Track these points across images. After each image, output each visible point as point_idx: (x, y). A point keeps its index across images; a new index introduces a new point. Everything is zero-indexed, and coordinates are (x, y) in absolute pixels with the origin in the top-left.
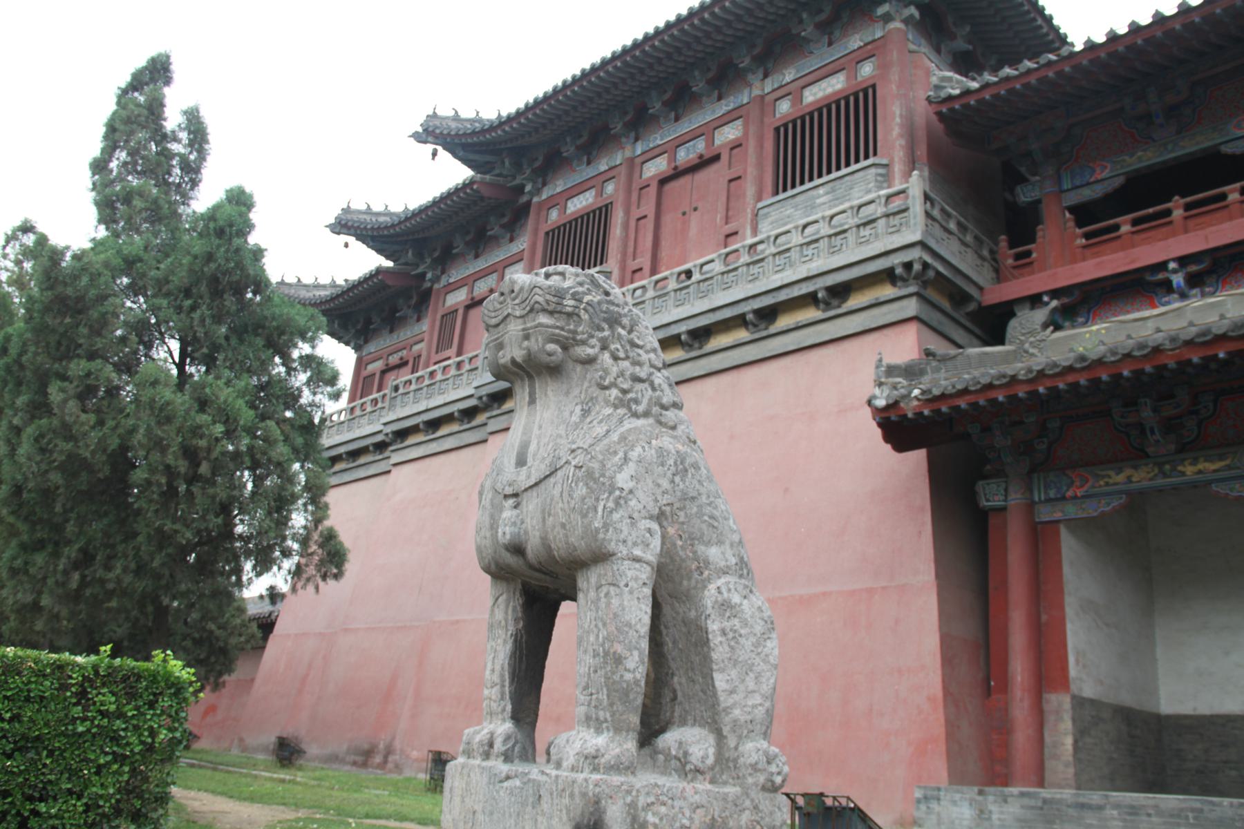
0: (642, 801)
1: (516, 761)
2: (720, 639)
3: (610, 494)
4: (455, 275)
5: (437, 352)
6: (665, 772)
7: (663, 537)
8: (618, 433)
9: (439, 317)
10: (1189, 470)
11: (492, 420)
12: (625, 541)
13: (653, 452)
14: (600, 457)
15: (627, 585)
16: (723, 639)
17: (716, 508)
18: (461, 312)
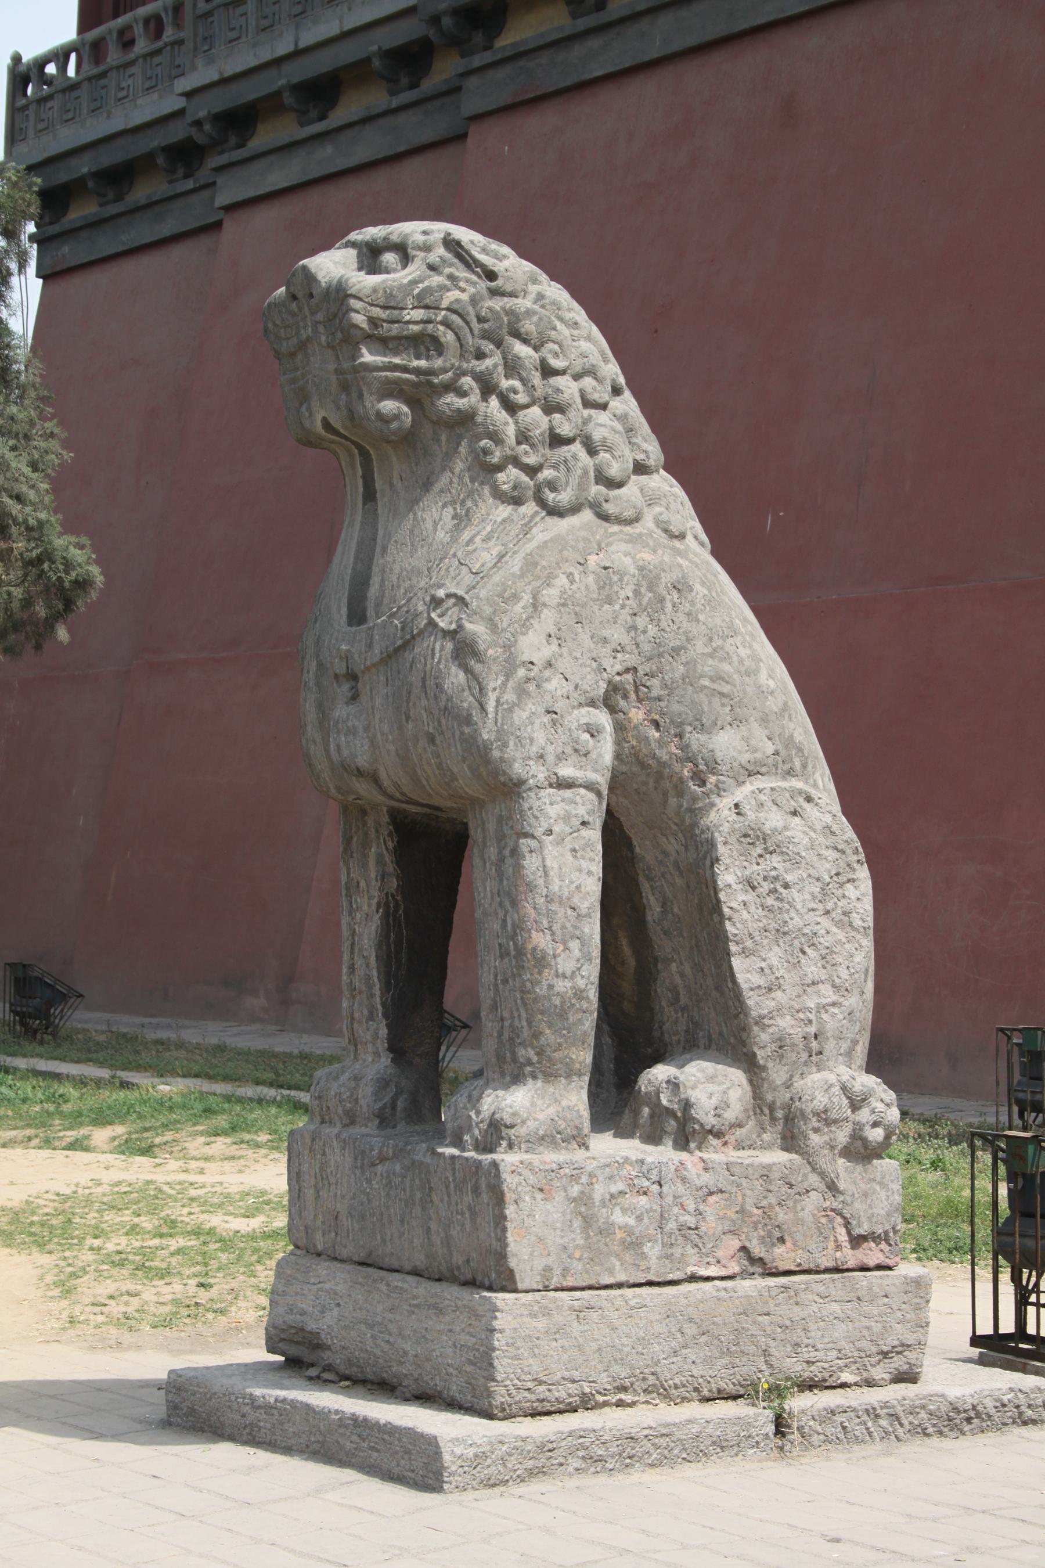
0: (600, 1191)
1: (401, 1126)
2: (742, 897)
3: (508, 677)
6: (653, 1138)
7: (620, 728)
8: (520, 556)
11: (473, 82)
12: (541, 757)
13: (591, 579)
14: (488, 610)
15: (549, 832)
16: (750, 897)
17: (727, 658)
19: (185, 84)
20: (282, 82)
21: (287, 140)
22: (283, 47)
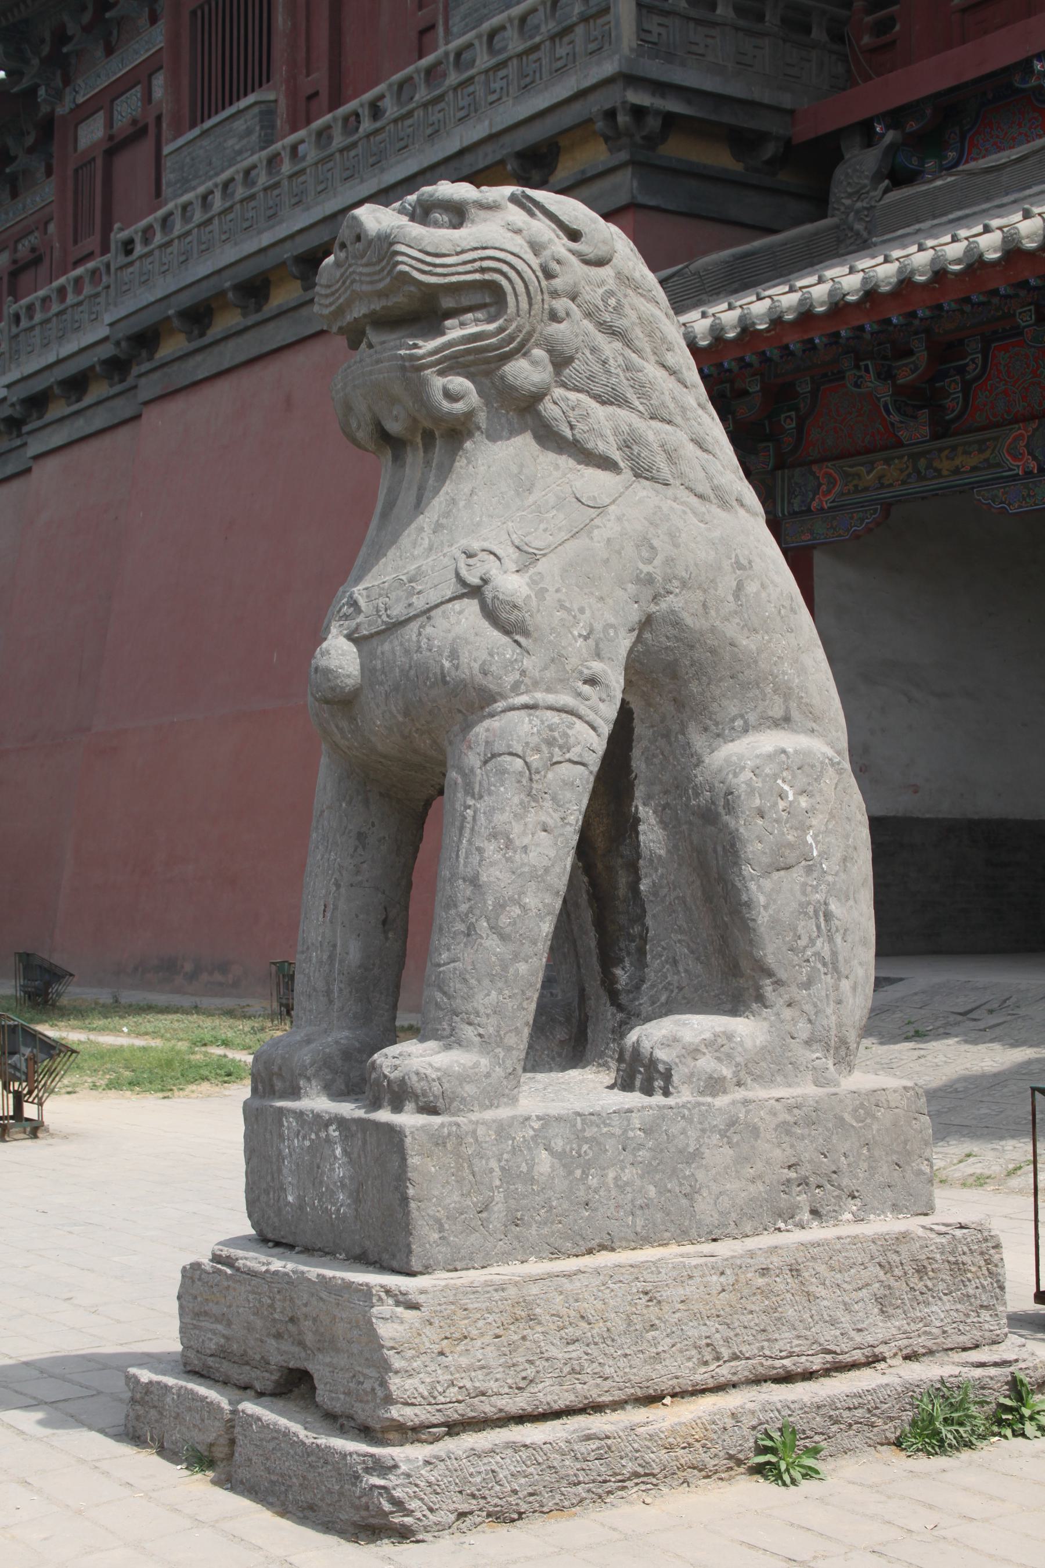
4: (84, 91)
5: (76, 242)
9: (70, 172)
10: (945, 465)
18: (99, 162)
19: (108, 319)
20: (52, 380)
21: (105, 396)
22: (51, 358)
